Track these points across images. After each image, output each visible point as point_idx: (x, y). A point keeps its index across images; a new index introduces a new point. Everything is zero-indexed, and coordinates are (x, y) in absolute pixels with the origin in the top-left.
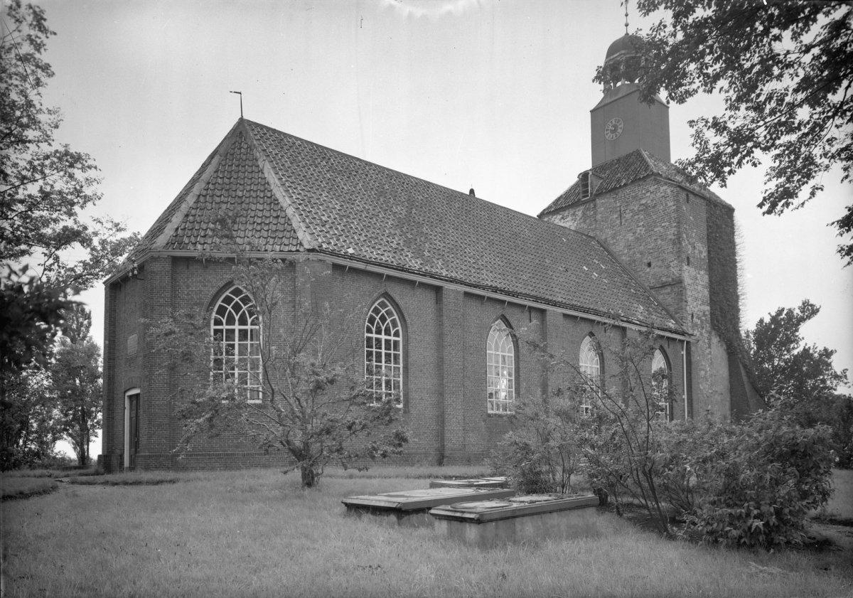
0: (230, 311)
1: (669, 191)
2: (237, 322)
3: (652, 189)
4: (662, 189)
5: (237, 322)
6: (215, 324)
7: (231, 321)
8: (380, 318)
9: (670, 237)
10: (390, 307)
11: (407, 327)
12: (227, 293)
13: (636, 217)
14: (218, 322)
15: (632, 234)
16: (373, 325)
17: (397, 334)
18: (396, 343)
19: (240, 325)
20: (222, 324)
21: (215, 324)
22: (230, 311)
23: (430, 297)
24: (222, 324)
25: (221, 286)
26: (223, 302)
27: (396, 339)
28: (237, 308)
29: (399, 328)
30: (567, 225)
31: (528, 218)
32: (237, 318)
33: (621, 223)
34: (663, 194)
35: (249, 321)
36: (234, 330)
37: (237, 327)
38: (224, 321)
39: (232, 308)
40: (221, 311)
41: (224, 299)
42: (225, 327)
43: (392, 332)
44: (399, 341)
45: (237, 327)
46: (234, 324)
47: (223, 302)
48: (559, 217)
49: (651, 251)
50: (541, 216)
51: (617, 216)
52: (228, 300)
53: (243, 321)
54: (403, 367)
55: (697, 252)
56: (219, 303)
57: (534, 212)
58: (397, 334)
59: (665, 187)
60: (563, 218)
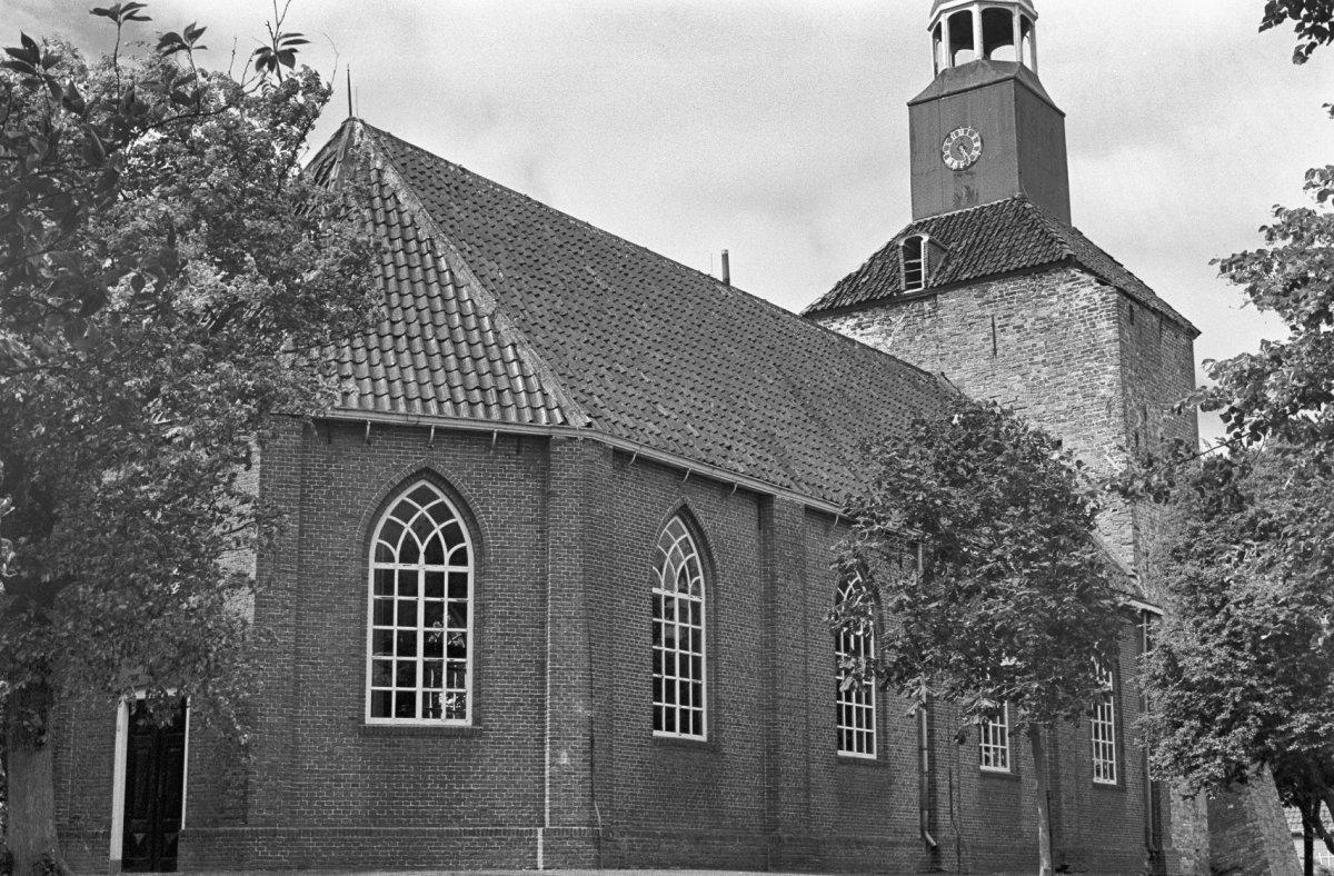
0: (408, 533)
1: (1096, 297)
2: (422, 558)
3: (1062, 289)
4: (1083, 292)
5: (422, 558)
6: (378, 559)
7: (409, 554)
8: (413, 526)
9: (1103, 391)
10: (443, 498)
11: (715, 576)
12: (403, 497)
13: (1029, 343)
14: (383, 555)
15: (1018, 378)
16: (844, 591)
17: (460, 558)
18: (696, 606)
19: (427, 562)
20: (391, 559)
21: (378, 559)
22: (408, 533)
23: (750, 512)
24: (391, 559)
25: (397, 482)
26: (392, 514)
27: (696, 599)
28: (423, 527)
29: (468, 543)
30: (870, 342)
31: (778, 314)
32: (422, 548)
33: (995, 350)
34: (1085, 303)
35: (447, 556)
36: (415, 573)
37: (422, 568)
38: (396, 554)
39: (442, 530)
40: (391, 532)
41: (396, 509)
42: (397, 566)
43: (447, 556)
44: (465, 575)
45: (422, 568)
46: (416, 562)
47: (392, 514)
48: (852, 322)
49: (1062, 417)
50: (812, 314)
51: (985, 335)
52: (405, 511)
53: (434, 556)
54: (708, 658)
55: (529, 214)
56: (387, 515)
57: (797, 303)
58: (696, 593)
59: (1089, 290)
60: (859, 325)
